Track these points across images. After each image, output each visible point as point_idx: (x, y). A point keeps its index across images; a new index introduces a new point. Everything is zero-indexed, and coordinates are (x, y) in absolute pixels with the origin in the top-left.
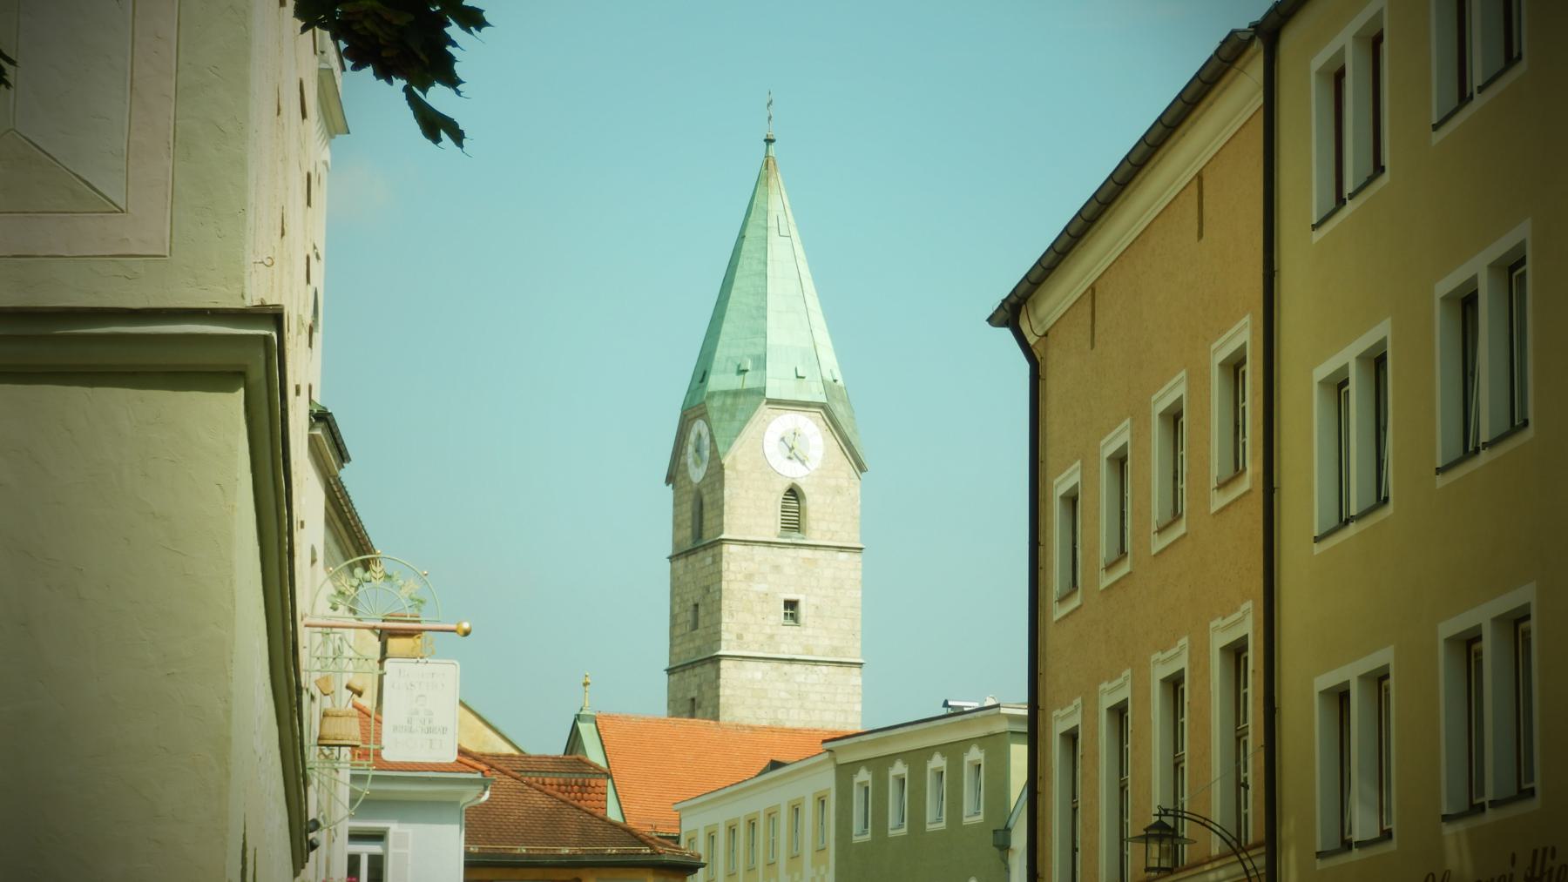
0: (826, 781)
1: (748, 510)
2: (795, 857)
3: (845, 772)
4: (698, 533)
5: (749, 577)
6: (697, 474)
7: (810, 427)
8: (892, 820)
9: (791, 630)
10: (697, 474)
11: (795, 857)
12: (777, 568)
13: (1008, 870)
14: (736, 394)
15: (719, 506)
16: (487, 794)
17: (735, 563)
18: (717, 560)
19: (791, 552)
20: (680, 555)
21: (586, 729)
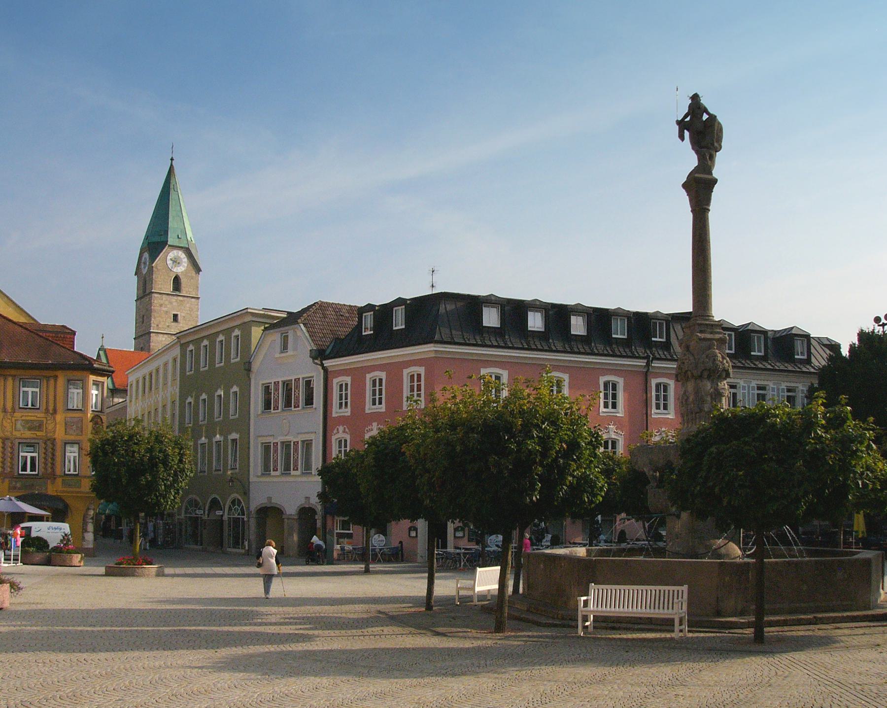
0: (177, 352)
1: (162, 284)
2: (165, 384)
3: (184, 346)
4: (144, 291)
5: (161, 305)
6: (145, 271)
7: (182, 255)
8: (202, 364)
9: (174, 324)
10: (145, 271)
11: (165, 384)
12: (171, 303)
13: (250, 379)
14: (158, 243)
15: (151, 280)
16: (725, 504)
17: (156, 300)
18: (150, 299)
19: (175, 298)
20: (139, 299)
21: (102, 353)
